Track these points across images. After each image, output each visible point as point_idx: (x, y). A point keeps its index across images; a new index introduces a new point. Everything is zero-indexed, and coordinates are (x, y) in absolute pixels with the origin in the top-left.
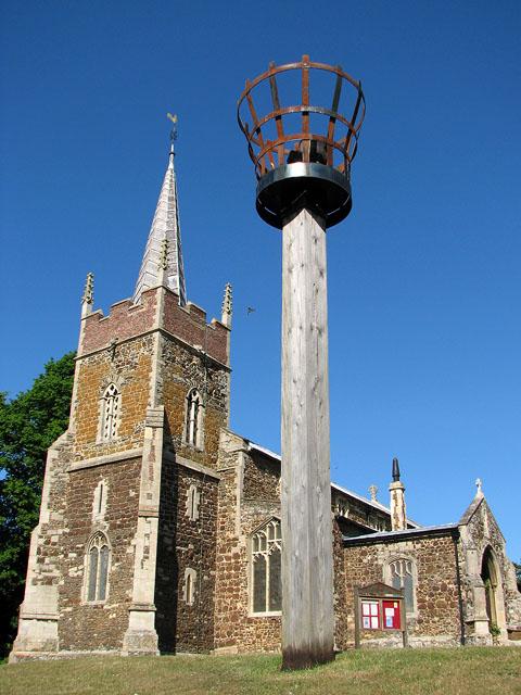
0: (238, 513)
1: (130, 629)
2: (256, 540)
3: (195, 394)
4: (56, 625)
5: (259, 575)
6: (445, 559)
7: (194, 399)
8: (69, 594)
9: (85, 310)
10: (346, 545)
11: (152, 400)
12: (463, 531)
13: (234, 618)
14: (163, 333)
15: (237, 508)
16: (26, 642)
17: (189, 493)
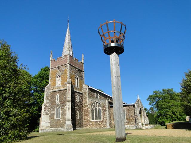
4: (49, 123)
7: (77, 78)
9: (51, 59)
11: (68, 78)
13: (88, 121)
14: (70, 64)
15: (87, 99)
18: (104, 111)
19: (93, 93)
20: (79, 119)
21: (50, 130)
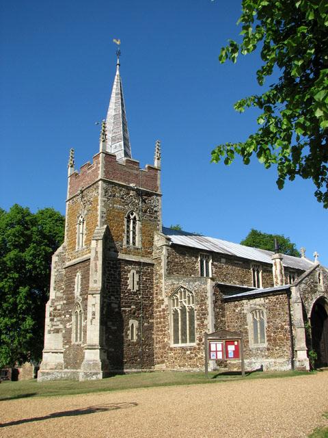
0: (163, 284)
1: (85, 360)
2: (174, 300)
3: (132, 214)
4: (62, 355)
5: (176, 321)
6: (283, 309)
7: (132, 217)
8: (67, 339)
9: (70, 171)
10: (227, 301)
11: (99, 223)
12: (294, 290)
13: (164, 347)
14: (104, 181)
15: (163, 281)
16: (46, 365)
17: (130, 275)
18: (204, 314)
19: (186, 260)
20: (138, 343)
21: (63, 376)
